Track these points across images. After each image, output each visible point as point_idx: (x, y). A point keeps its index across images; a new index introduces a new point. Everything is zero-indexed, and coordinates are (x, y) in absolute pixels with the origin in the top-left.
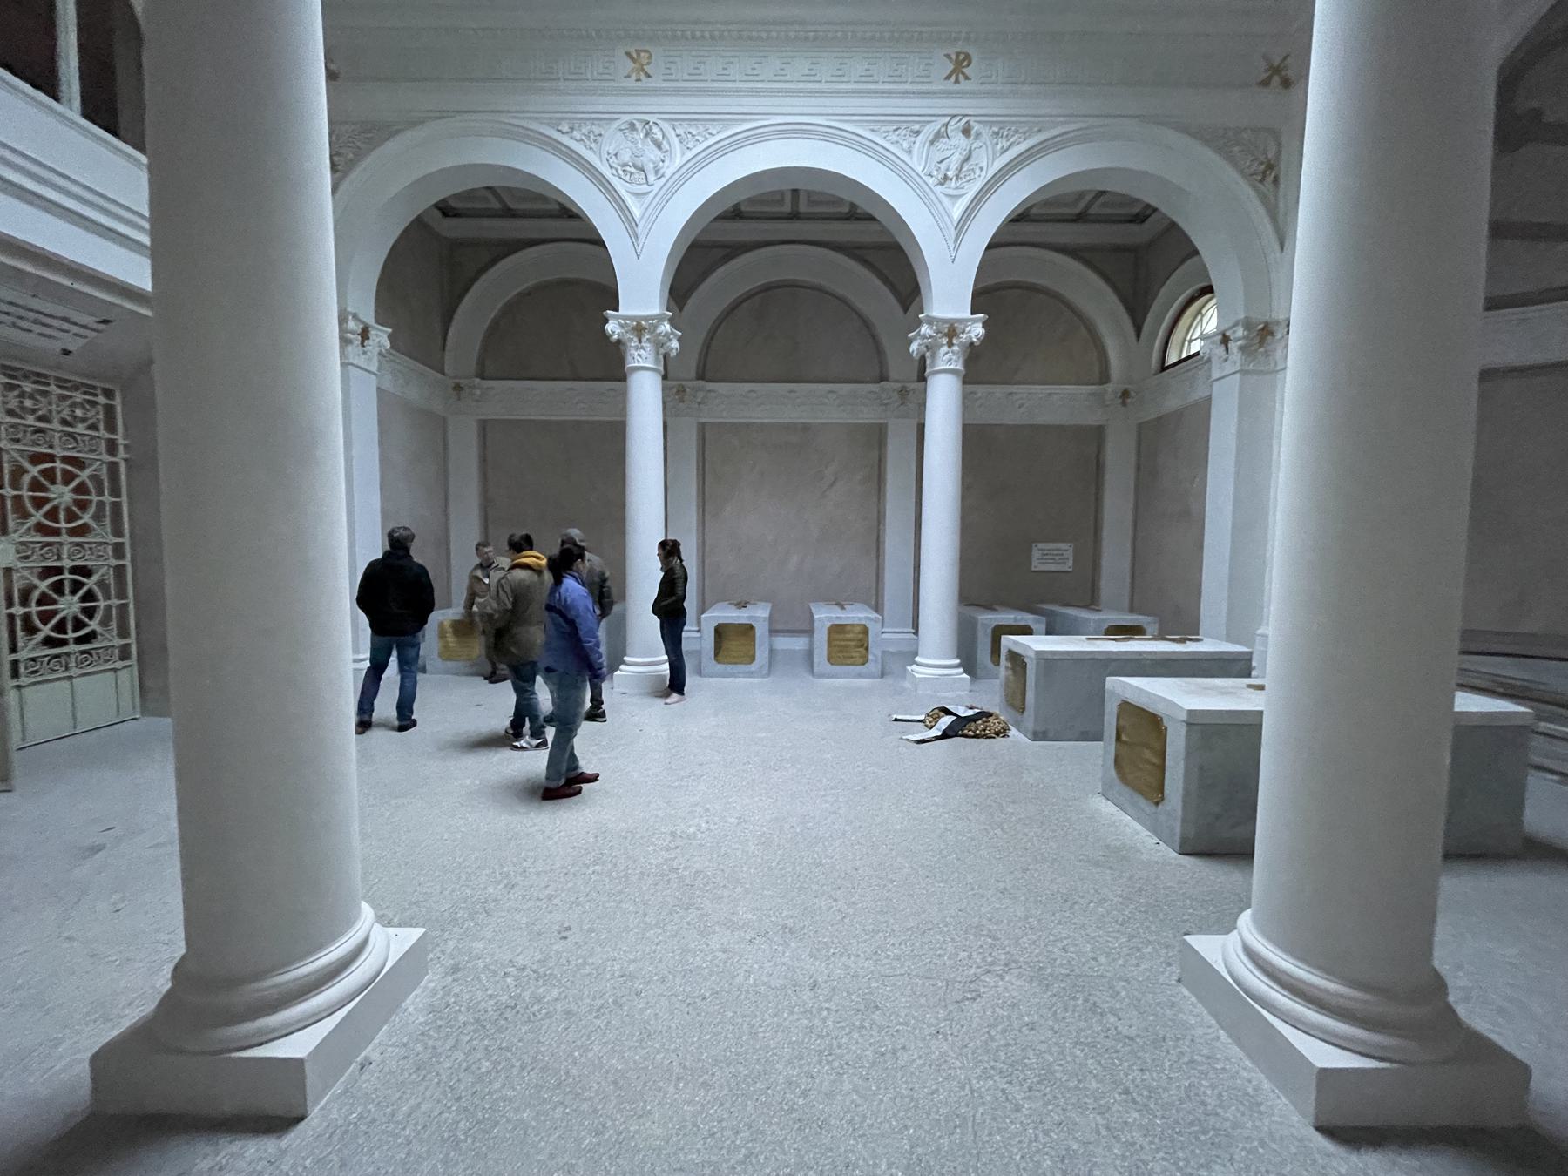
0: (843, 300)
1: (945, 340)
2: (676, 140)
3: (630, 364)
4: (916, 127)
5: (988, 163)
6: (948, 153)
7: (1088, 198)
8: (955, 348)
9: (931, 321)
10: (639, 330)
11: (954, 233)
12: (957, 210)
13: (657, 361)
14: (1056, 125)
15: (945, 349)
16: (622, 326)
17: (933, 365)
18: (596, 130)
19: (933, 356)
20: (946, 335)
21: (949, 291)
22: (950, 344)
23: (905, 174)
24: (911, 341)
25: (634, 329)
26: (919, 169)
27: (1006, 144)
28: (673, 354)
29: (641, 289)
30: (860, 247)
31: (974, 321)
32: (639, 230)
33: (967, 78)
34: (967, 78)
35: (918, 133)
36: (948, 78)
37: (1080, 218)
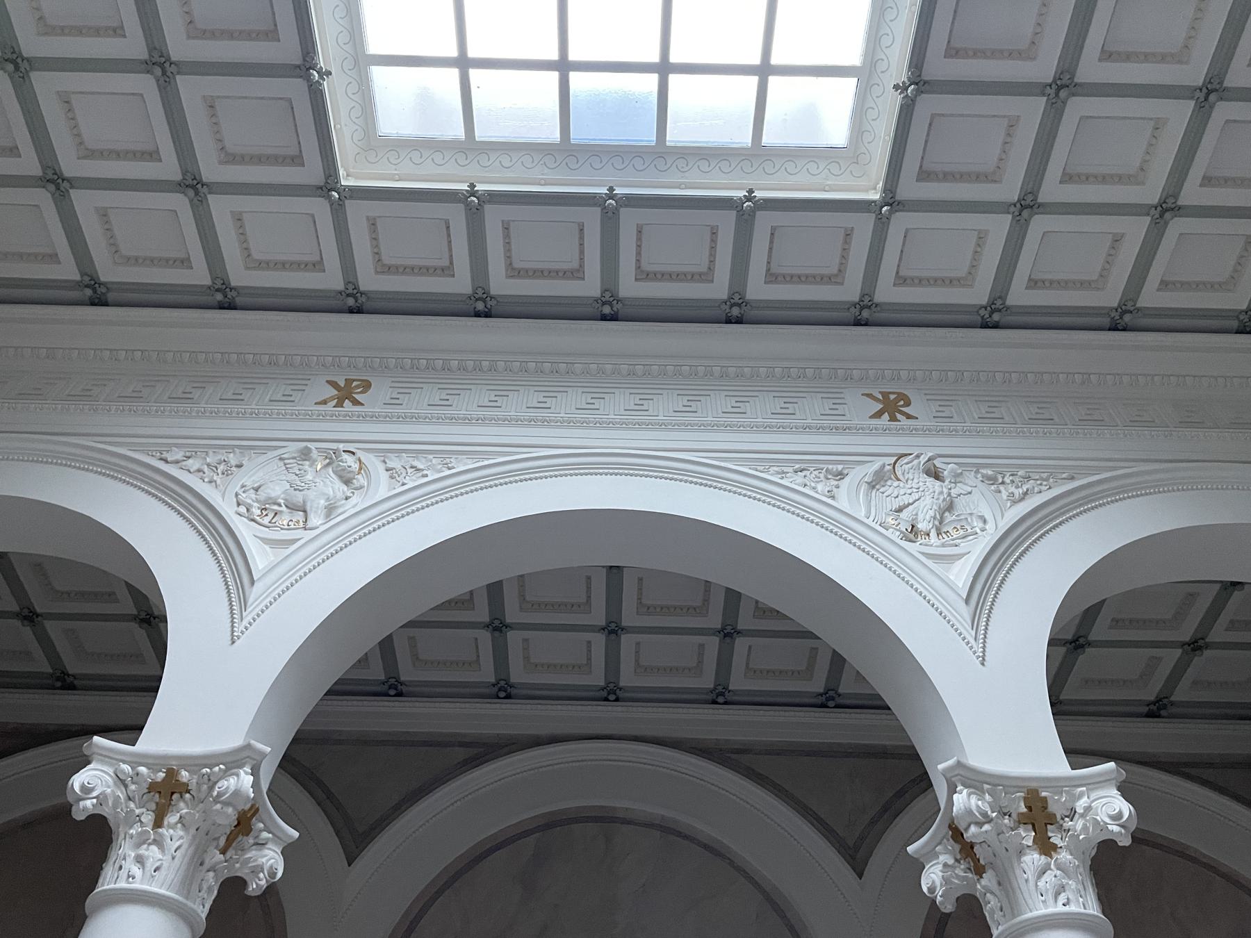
0: (714, 850)
1: (1028, 837)
2: (384, 476)
3: (110, 881)
4: (840, 467)
5: (990, 514)
6: (907, 499)
7: (1203, 604)
8: (1064, 856)
9: (976, 780)
10: (167, 790)
11: (966, 612)
12: (961, 574)
13: (188, 882)
14: (1099, 470)
15: (1033, 859)
16: (121, 781)
17: (1011, 904)
18: (233, 459)
19: (1006, 884)
20: (1023, 820)
21: (991, 714)
22: (1046, 847)
23: (839, 526)
24: (918, 867)
25: (153, 787)
26: (861, 515)
27: (1018, 492)
28: (257, 885)
29: (222, 692)
30: (744, 750)
31: (1094, 784)
32: (254, 593)
33: (909, 417)
34: (909, 417)
35: (841, 475)
36: (878, 415)
37: (1157, 710)
